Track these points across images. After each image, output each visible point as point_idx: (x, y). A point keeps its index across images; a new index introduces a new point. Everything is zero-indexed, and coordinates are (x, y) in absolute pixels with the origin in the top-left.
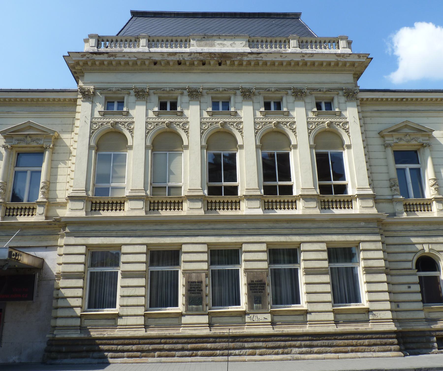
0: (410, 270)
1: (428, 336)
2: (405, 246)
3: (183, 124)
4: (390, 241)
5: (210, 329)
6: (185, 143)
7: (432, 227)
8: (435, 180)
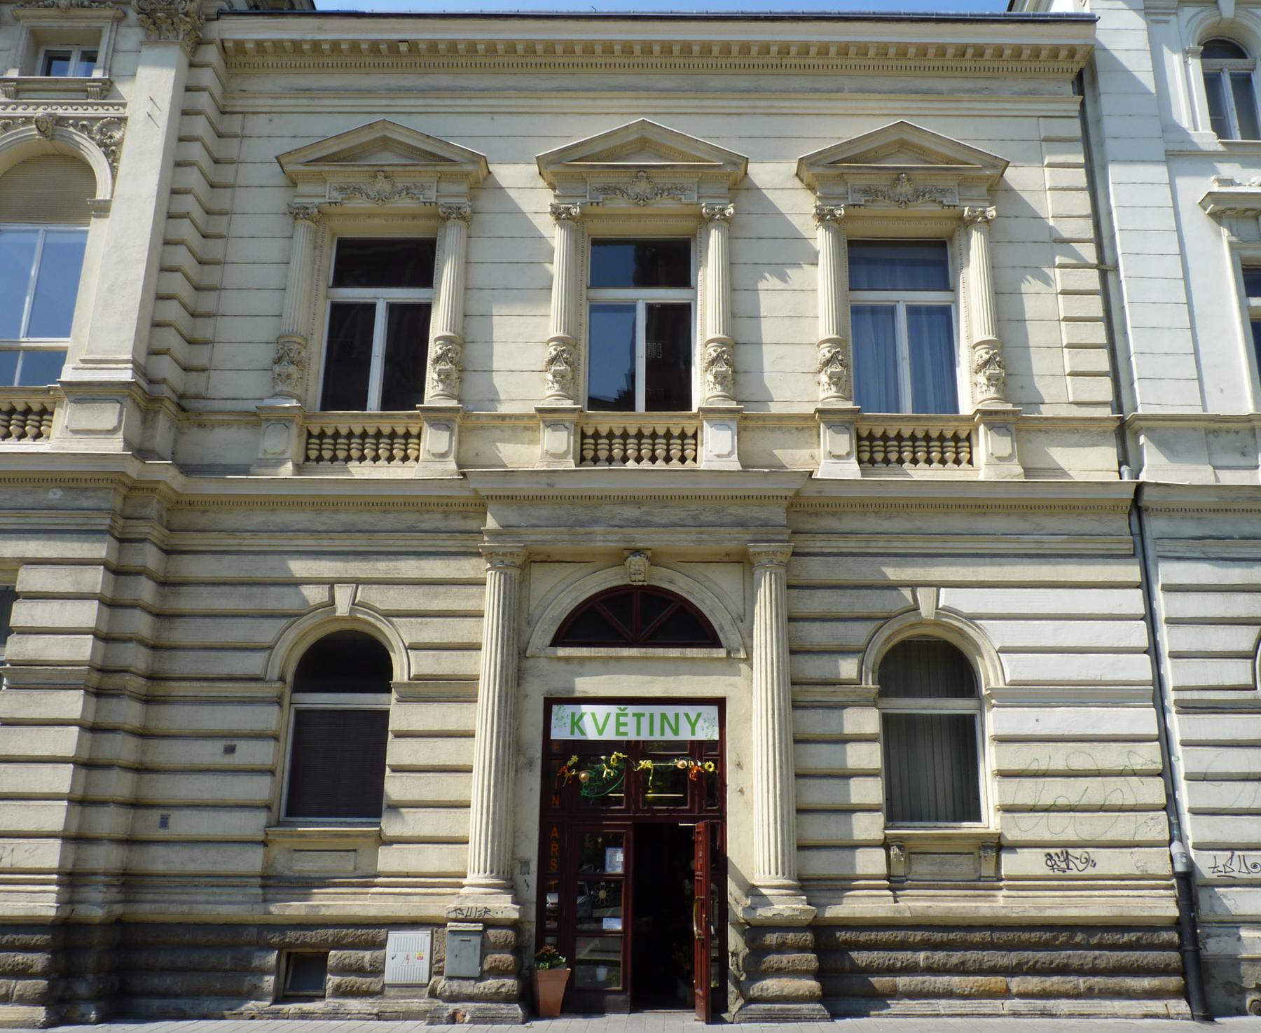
0: (260, 685)
1: (249, 944)
2: (255, 589)
3: (104, 125)
4: (815, 569)
5: (895, 897)
6: (102, 193)
7: (389, 521)
8: (560, 341)
